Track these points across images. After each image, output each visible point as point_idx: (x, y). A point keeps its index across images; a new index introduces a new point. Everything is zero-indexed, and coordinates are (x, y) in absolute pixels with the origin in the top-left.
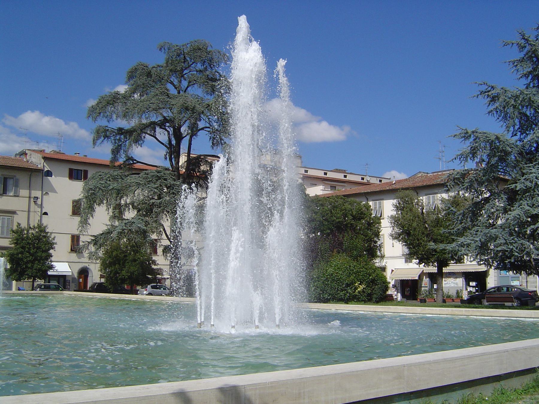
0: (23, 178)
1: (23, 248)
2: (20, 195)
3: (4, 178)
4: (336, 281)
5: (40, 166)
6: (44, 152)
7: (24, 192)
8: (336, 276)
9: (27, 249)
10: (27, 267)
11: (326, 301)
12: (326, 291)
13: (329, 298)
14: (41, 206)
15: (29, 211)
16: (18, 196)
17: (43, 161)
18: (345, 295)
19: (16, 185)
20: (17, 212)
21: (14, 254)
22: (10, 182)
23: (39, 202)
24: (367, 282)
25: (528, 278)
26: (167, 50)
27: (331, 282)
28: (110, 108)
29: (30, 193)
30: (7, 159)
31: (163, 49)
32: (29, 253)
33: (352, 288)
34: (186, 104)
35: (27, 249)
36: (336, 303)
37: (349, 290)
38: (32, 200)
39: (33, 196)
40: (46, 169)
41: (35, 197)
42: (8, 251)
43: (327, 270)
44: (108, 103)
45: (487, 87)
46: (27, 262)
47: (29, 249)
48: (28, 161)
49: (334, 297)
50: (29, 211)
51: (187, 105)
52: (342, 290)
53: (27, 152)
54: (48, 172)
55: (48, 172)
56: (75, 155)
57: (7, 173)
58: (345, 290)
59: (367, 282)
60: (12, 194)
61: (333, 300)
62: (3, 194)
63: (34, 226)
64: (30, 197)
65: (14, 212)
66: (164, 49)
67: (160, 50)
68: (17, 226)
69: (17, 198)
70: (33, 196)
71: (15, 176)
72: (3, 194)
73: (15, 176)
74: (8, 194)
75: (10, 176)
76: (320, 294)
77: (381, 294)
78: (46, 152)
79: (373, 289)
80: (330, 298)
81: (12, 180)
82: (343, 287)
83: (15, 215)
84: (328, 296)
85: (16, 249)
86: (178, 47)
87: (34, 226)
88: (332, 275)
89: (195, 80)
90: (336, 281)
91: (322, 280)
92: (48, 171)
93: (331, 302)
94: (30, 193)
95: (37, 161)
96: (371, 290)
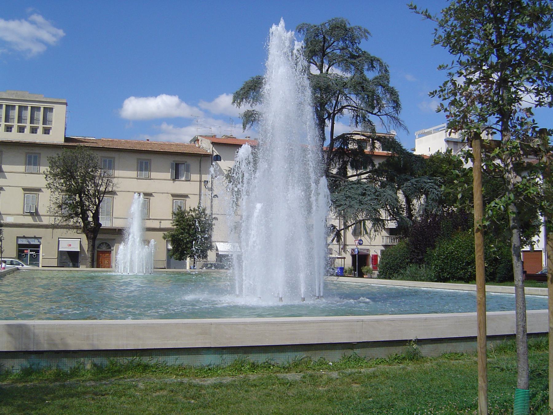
0: (193, 164)
1: (184, 229)
2: (191, 179)
3: (176, 164)
4: (456, 260)
5: (209, 152)
6: (215, 137)
7: (195, 177)
8: (456, 254)
9: (186, 230)
10: (186, 247)
11: (445, 280)
12: (445, 270)
13: (448, 276)
14: (211, 189)
15: (200, 195)
16: (189, 181)
17: (212, 146)
18: (465, 273)
19: (188, 170)
20: (153, 194)
21: (175, 235)
22: (182, 168)
23: (209, 185)
24: (489, 261)
25: (161, 234)
26: (306, 31)
27: (451, 261)
28: (252, 93)
29: (201, 178)
30: (180, 145)
31: (302, 30)
32: (189, 234)
33: (472, 267)
34: (319, 84)
35: (186, 230)
36: (455, 282)
37: (470, 269)
38: (203, 183)
39: (203, 180)
40: (215, 154)
41: (205, 181)
42: (169, 231)
43: (447, 248)
44: (249, 88)
45: (311, 64)
46: (187, 243)
47: (189, 230)
48: (199, 147)
49: (454, 275)
50: (200, 195)
51: (320, 85)
52: (462, 269)
53: (199, 138)
54: (217, 157)
55: (217, 157)
56: (246, 139)
57: (178, 159)
58: (466, 269)
59: (489, 261)
60: (183, 179)
61: (453, 279)
62: (175, 178)
63: (194, 209)
64: (200, 181)
65: (186, 196)
66: (303, 30)
67: (299, 32)
68: (178, 209)
69: (189, 182)
70: (203, 180)
71: (186, 162)
72: (175, 178)
73: (186, 162)
74: (180, 179)
75: (180, 161)
76: (439, 272)
77: (505, 273)
78: (217, 137)
79: (497, 268)
80: (449, 277)
81: (184, 165)
82: (463, 266)
83: (187, 199)
84: (448, 275)
85: (176, 230)
86: (316, 27)
87: (194, 209)
88: (452, 253)
89: (334, 60)
90: (456, 260)
91: (441, 258)
92: (217, 155)
93: (451, 281)
94: (201, 178)
95: (206, 146)
96: (494, 269)
